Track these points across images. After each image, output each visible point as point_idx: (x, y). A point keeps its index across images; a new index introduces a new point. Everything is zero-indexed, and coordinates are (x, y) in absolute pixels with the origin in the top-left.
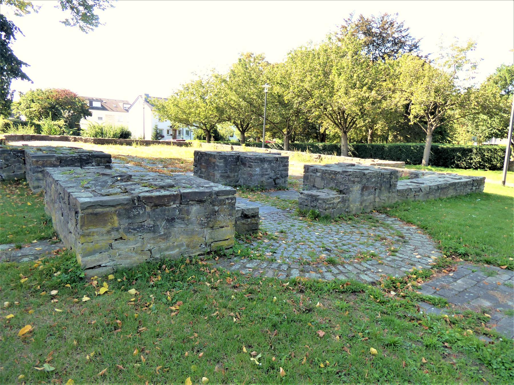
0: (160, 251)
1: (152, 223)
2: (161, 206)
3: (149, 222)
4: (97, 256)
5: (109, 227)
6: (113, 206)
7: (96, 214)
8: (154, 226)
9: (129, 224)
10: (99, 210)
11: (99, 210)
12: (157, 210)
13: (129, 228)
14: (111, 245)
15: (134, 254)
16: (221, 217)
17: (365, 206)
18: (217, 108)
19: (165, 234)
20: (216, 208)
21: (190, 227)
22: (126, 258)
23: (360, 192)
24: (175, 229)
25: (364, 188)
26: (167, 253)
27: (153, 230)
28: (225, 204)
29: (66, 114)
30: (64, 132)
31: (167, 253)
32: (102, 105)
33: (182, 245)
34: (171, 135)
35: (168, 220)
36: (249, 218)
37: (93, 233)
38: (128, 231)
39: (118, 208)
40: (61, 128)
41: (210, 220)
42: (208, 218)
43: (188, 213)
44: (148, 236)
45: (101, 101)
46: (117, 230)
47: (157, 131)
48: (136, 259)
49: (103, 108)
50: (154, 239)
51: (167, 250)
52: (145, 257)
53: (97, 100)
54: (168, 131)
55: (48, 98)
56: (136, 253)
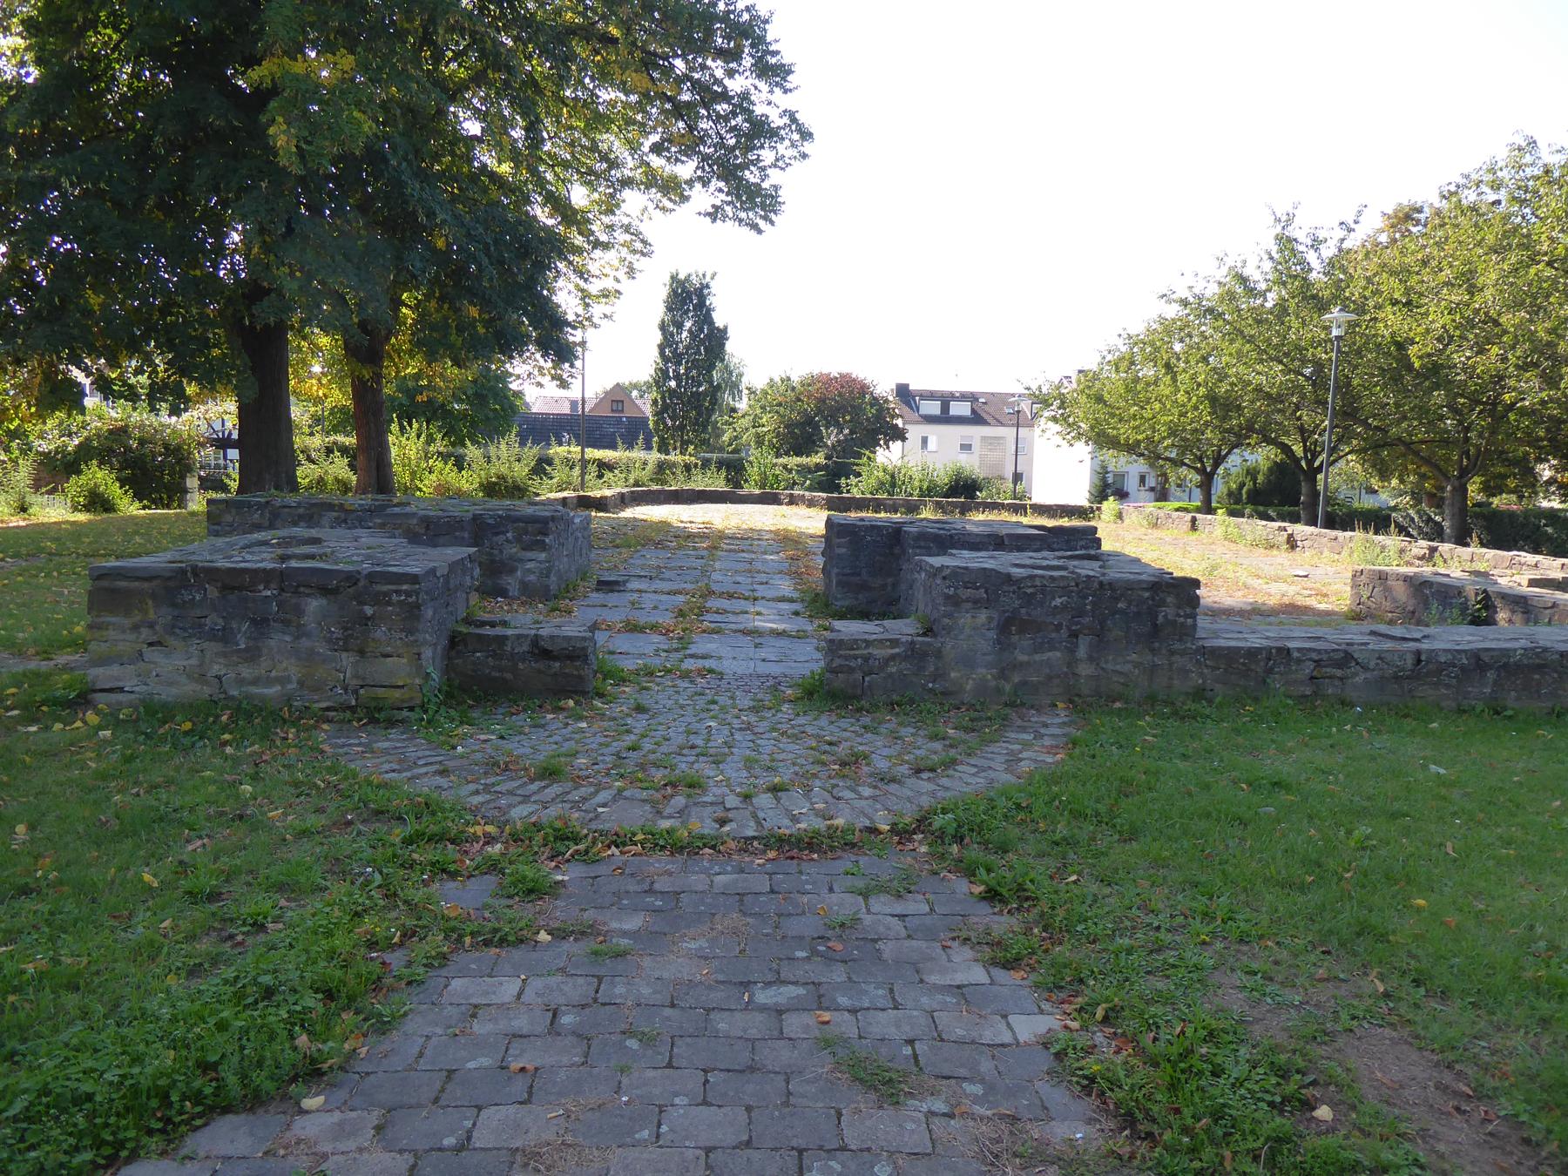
0: (241, 682)
1: (221, 621)
2: (240, 589)
3: (214, 621)
4: (115, 670)
5: (137, 617)
6: (138, 579)
7: (114, 591)
8: (224, 629)
9: (176, 618)
10: (123, 584)
11: (123, 584)
12: (230, 597)
13: (173, 627)
14: (141, 654)
15: (183, 679)
16: (380, 632)
17: (1024, 683)
18: (1212, 399)
19: (247, 650)
20: (369, 610)
21: (305, 643)
22: (171, 684)
23: (992, 635)
24: (272, 643)
25: (1008, 626)
26: (255, 690)
27: (224, 636)
28: (389, 603)
29: (832, 437)
30: (795, 483)
31: (255, 690)
32: (973, 411)
33: (288, 680)
34: (1152, 489)
35: (254, 622)
36: (555, 658)
37: (109, 624)
38: (171, 629)
39: (155, 583)
40: (790, 471)
41: (354, 636)
42: (346, 629)
43: (299, 612)
44: (212, 647)
45: (972, 398)
46: (151, 626)
47: (1104, 479)
48: (187, 689)
49: (976, 419)
50: (225, 655)
51: (255, 682)
52: (207, 690)
53: (964, 397)
54: (1142, 479)
55: (799, 400)
56: (189, 676)
